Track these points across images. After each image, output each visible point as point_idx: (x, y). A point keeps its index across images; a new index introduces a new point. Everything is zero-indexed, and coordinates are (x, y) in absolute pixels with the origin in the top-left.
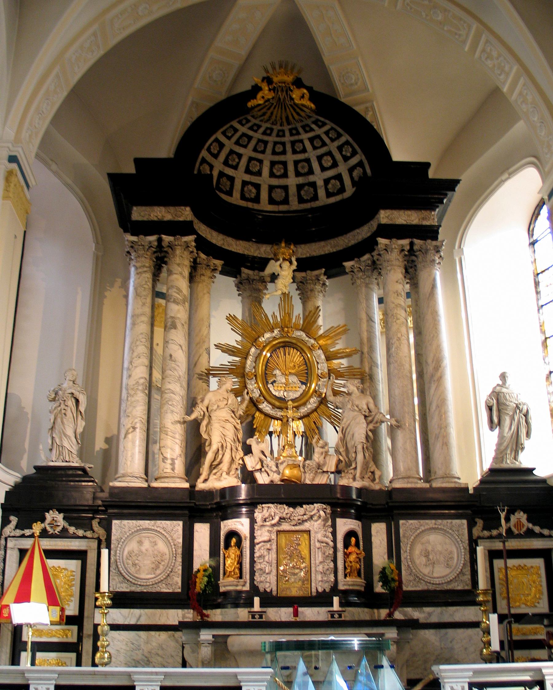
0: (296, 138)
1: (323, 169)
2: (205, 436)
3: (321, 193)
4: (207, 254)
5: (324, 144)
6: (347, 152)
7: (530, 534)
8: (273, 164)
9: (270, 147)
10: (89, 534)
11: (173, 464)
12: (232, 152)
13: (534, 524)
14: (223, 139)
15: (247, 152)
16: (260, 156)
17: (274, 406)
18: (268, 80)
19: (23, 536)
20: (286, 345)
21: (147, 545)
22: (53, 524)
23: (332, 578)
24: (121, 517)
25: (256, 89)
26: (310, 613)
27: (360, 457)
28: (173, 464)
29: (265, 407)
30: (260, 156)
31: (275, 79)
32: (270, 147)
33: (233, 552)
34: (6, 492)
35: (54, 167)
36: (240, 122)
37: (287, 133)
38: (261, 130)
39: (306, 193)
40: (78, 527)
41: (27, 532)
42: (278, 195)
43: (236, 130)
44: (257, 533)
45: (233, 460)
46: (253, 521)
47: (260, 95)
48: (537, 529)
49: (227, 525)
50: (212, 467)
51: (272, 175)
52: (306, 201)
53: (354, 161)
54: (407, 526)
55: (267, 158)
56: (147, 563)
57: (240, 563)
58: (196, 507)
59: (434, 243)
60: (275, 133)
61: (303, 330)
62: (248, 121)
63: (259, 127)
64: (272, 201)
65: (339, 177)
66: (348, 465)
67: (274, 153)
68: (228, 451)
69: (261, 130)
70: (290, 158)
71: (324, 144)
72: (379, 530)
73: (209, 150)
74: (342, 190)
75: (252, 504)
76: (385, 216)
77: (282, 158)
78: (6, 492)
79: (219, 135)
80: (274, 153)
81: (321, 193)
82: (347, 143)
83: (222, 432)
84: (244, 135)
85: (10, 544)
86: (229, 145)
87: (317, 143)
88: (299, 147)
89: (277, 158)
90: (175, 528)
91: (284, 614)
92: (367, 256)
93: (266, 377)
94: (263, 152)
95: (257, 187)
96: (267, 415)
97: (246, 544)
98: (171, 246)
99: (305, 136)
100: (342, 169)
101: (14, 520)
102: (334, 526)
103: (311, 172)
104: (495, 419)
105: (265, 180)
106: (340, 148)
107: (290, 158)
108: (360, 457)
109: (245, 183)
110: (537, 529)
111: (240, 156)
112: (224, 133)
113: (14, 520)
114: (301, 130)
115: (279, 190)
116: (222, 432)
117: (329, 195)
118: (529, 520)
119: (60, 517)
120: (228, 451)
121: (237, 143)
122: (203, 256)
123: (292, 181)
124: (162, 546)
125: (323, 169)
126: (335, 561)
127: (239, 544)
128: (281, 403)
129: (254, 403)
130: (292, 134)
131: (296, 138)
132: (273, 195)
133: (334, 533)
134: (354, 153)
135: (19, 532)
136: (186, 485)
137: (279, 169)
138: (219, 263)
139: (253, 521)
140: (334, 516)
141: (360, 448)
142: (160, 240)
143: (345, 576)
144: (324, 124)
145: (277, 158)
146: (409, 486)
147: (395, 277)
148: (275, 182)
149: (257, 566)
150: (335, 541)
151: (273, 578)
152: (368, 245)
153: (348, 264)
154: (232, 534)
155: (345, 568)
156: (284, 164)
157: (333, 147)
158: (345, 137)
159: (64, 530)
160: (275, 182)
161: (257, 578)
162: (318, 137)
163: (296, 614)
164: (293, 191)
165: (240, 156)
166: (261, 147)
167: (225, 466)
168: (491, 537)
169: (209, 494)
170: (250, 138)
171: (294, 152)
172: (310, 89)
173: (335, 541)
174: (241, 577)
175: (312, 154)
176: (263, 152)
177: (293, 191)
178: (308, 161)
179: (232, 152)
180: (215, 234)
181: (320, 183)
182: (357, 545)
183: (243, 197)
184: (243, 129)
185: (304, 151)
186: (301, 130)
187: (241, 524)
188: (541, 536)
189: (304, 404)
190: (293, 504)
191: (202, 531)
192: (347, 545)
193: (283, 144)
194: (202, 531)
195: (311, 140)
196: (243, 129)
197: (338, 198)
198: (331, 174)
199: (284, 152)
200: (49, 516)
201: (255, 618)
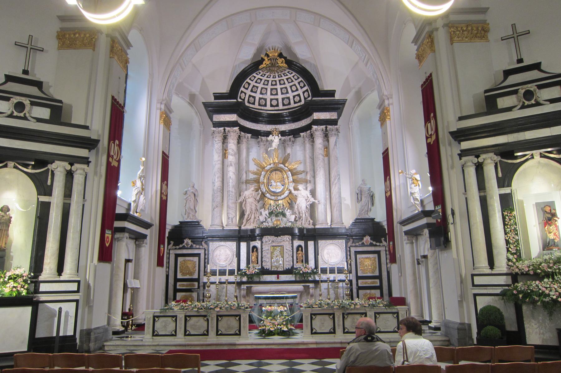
0: (281, 78)
1: (293, 91)
2: (244, 208)
3: (292, 102)
4: (245, 132)
5: (292, 81)
6: (302, 85)
7: (371, 245)
8: (272, 89)
9: (270, 82)
10: (201, 247)
11: (232, 220)
12: (254, 86)
13: (374, 241)
14: (250, 81)
15: (261, 86)
16: (266, 87)
17: (271, 195)
18: (267, 55)
19: (176, 249)
20: (276, 170)
21: (222, 251)
22: (187, 244)
23: (292, 264)
24: (212, 241)
25: (263, 60)
26: (283, 277)
27: (304, 216)
28: (232, 220)
29: (268, 195)
30: (266, 87)
31: (270, 55)
32: (270, 82)
33: (255, 254)
34: (49, 82)
35: (180, 96)
36: (257, 74)
37: (277, 77)
38: (266, 76)
39: (286, 102)
40: (196, 244)
41: (177, 247)
42: (274, 103)
43: (255, 77)
44: (263, 247)
45: (255, 218)
46: (262, 243)
47: (264, 63)
48: (374, 243)
49: (253, 244)
50: (247, 221)
51: (271, 94)
52: (286, 105)
53: (305, 89)
54: (321, 243)
55: (269, 87)
56: (223, 257)
57: (257, 258)
58: (240, 236)
59: (336, 126)
60: (272, 76)
61: (282, 164)
62: (260, 73)
63: (265, 75)
64: (272, 106)
65: (299, 95)
66: (300, 218)
67: (272, 85)
68: (253, 214)
69: (266, 76)
70: (279, 87)
71: (292, 81)
72: (311, 244)
73: (244, 87)
74: (300, 101)
75: (261, 236)
76: (317, 116)
77: (275, 87)
78: (49, 82)
79: (248, 80)
80: (272, 85)
81: (292, 102)
82: (302, 81)
83: (251, 204)
84: (259, 79)
85: (171, 252)
86: (253, 83)
87: (290, 80)
88: (282, 82)
89: (273, 87)
90: (233, 245)
91: (273, 278)
92: (309, 131)
93: (269, 184)
94: (267, 85)
95: (265, 100)
96: (268, 198)
97: (259, 251)
98: (229, 132)
99: (284, 78)
100: (300, 92)
101: (172, 242)
102: (292, 243)
103: (287, 93)
104: (359, 199)
105: (268, 97)
106: (299, 83)
107: (279, 87)
108: (304, 216)
109: (260, 99)
110: (374, 243)
111: (257, 87)
112: (250, 79)
113: (172, 242)
114: (282, 75)
115: (274, 101)
116: (251, 204)
117: (295, 103)
118: (371, 239)
119: (190, 241)
120: (253, 214)
121: (256, 82)
122: (242, 133)
123: (280, 97)
124: (228, 252)
125: (293, 91)
126: (293, 257)
127: (257, 250)
128: (275, 194)
129: (263, 195)
130: (279, 77)
131: (281, 78)
132: (272, 103)
133: (292, 246)
134: (305, 86)
135: (174, 247)
136: (237, 228)
137: (274, 92)
138: (250, 135)
139: (262, 243)
140: (292, 240)
141: (304, 212)
142: (224, 129)
143: (297, 262)
144: (292, 73)
145: (273, 87)
146: (322, 227)
147: (319, 141)
148: (273, 97)
149: (263, 259)
150: (293, 249)
151: (269, 264)
152: (308, 128)
153: (302, 134)
154: (254, 247)
155: (297, 259)
156: (276, 89)
157: (296, 82)
158: (301, 79)
159: (192, 246)
160: (273, 97)
161: (264, 264)
162: (290, 78)
163: (278, 278)
164: (280, 101)
165: (257, 87)
166: (266, 83)
167: (252, 220)
168: (356, 246)
169: (246, 231)
170: (261, 80)
171: (280, 84)
172: (285, 58)
173: (293, 249)
174: (257, 263)
175: (288, 85)
176: (267, 85)
177: (280, 101)
178: (286, 88)
179: (254, 86)
180: (248, 123)
181: (291, 98)
182: (302, 250)
183: (260, 105)
184: (258, 77)
185: (284, 84)
186: (282, 75)
187: (257, 243)
188: (376, 245)
189: (283, 194)
190: (277, 236)
191: (243, 245)
192: (298, 250)
193: (276, 81)
194: (243, 245)
195: (287, 79)
196: (258, 77)
197: (299, 104)
198: (295, 92)
199: (276, 85)
200: (186, 241)
201: (536, 86)
